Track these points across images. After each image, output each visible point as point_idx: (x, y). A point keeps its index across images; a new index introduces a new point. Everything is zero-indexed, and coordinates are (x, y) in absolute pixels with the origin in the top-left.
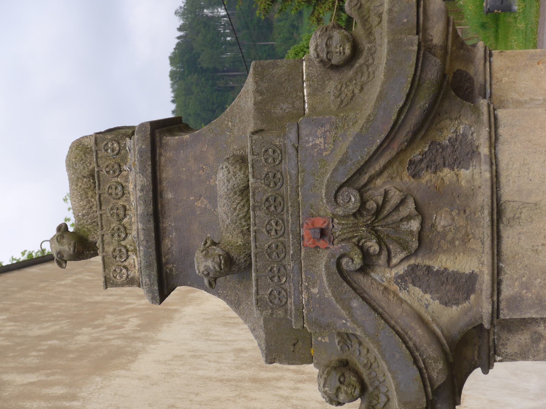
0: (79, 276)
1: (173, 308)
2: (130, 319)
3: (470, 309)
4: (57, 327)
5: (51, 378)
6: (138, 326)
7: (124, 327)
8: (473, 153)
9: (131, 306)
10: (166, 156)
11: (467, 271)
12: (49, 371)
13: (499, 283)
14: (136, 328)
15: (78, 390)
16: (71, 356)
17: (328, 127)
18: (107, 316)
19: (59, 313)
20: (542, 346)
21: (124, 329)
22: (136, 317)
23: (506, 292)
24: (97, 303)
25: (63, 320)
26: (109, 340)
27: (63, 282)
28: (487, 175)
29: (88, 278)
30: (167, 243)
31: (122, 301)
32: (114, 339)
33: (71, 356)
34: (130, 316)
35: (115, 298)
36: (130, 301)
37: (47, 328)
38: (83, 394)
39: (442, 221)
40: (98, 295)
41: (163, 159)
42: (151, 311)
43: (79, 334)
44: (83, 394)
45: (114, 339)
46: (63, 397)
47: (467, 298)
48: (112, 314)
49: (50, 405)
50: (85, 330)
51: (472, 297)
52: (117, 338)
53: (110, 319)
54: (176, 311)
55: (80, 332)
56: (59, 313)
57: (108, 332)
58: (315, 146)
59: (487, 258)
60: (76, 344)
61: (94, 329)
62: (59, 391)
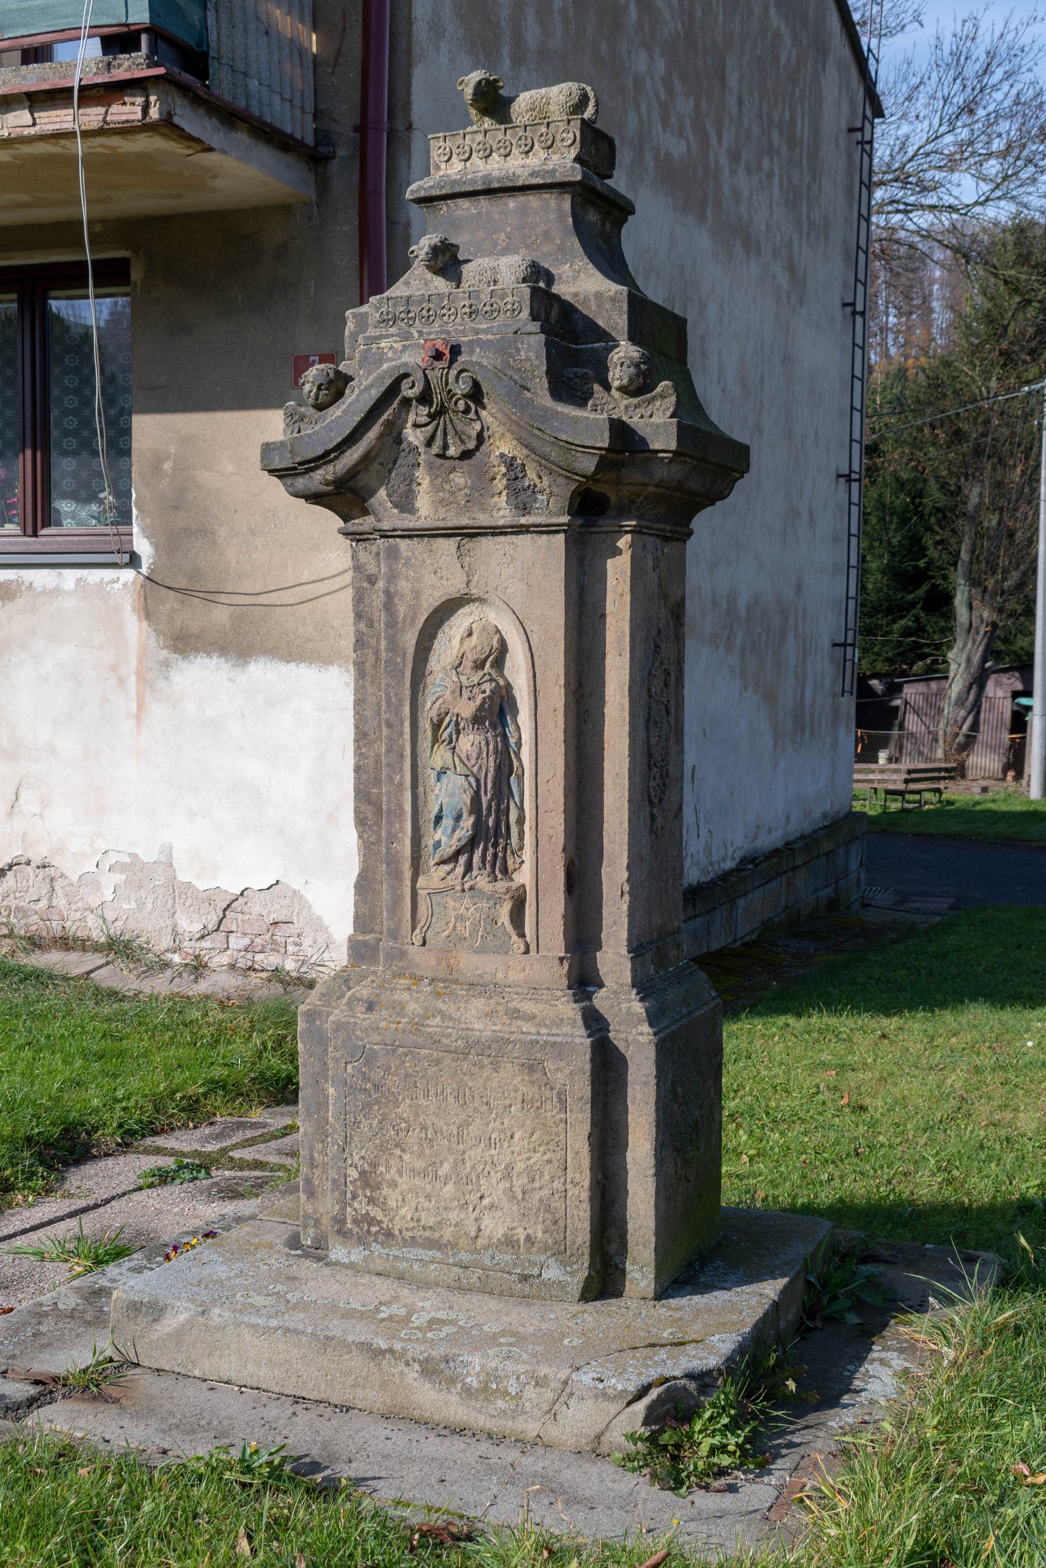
0: (788, 40)
1: (709, 212)
2: (683, 141)
3: (386, 510)
4: (667, 15)
5: (557, 18)
6: (668, 155)
7: (665, 131)
8: (525, 509)
9: (714, 140)
10: (551, 199)
11: (418, 504)
12: (571, 13)
13: (410, 537)
14: (663, 152)
15: (533, 65)
16: (604, 46)
17: (536, 363)
18: (692, 100)
19: (699, 13)
20: (365, 585)
21: (661, 131)
22: (689, 150)
23: (403, 544)
24: (723, 79)
25: (683, 23)
26: (638, 107)
27: (772, 11)
28: (501, 523)
29: (783, 57)
30: (465, 203)
31: (726, 123)
32: (639, 115)
33: (604, 46)
34: (692, 139)
35: (735, 111)
36: (725, 137)
37: (102, 146)
38: (524, 74)
39: (459, 479)
40: (741, 79)
41: (548, 196)
42: (701, 174)
43: (651, 55)
44: (524, 74)
45: (639, 115)
46: (518, 42)
47: (396, 506)
48: (697, 108)
49: (503, 24)
50: (660, 65)
51: (395, 511)
52: (641, 123)
53: (684, 106)
54: (701, 217)
55: (657, 56)
56: (699, 13)
57: (655, 105)
58: (518, 350)
59: (429, 524)
60: (629, 52)
61: (662, 79)
62: (532, 34)
